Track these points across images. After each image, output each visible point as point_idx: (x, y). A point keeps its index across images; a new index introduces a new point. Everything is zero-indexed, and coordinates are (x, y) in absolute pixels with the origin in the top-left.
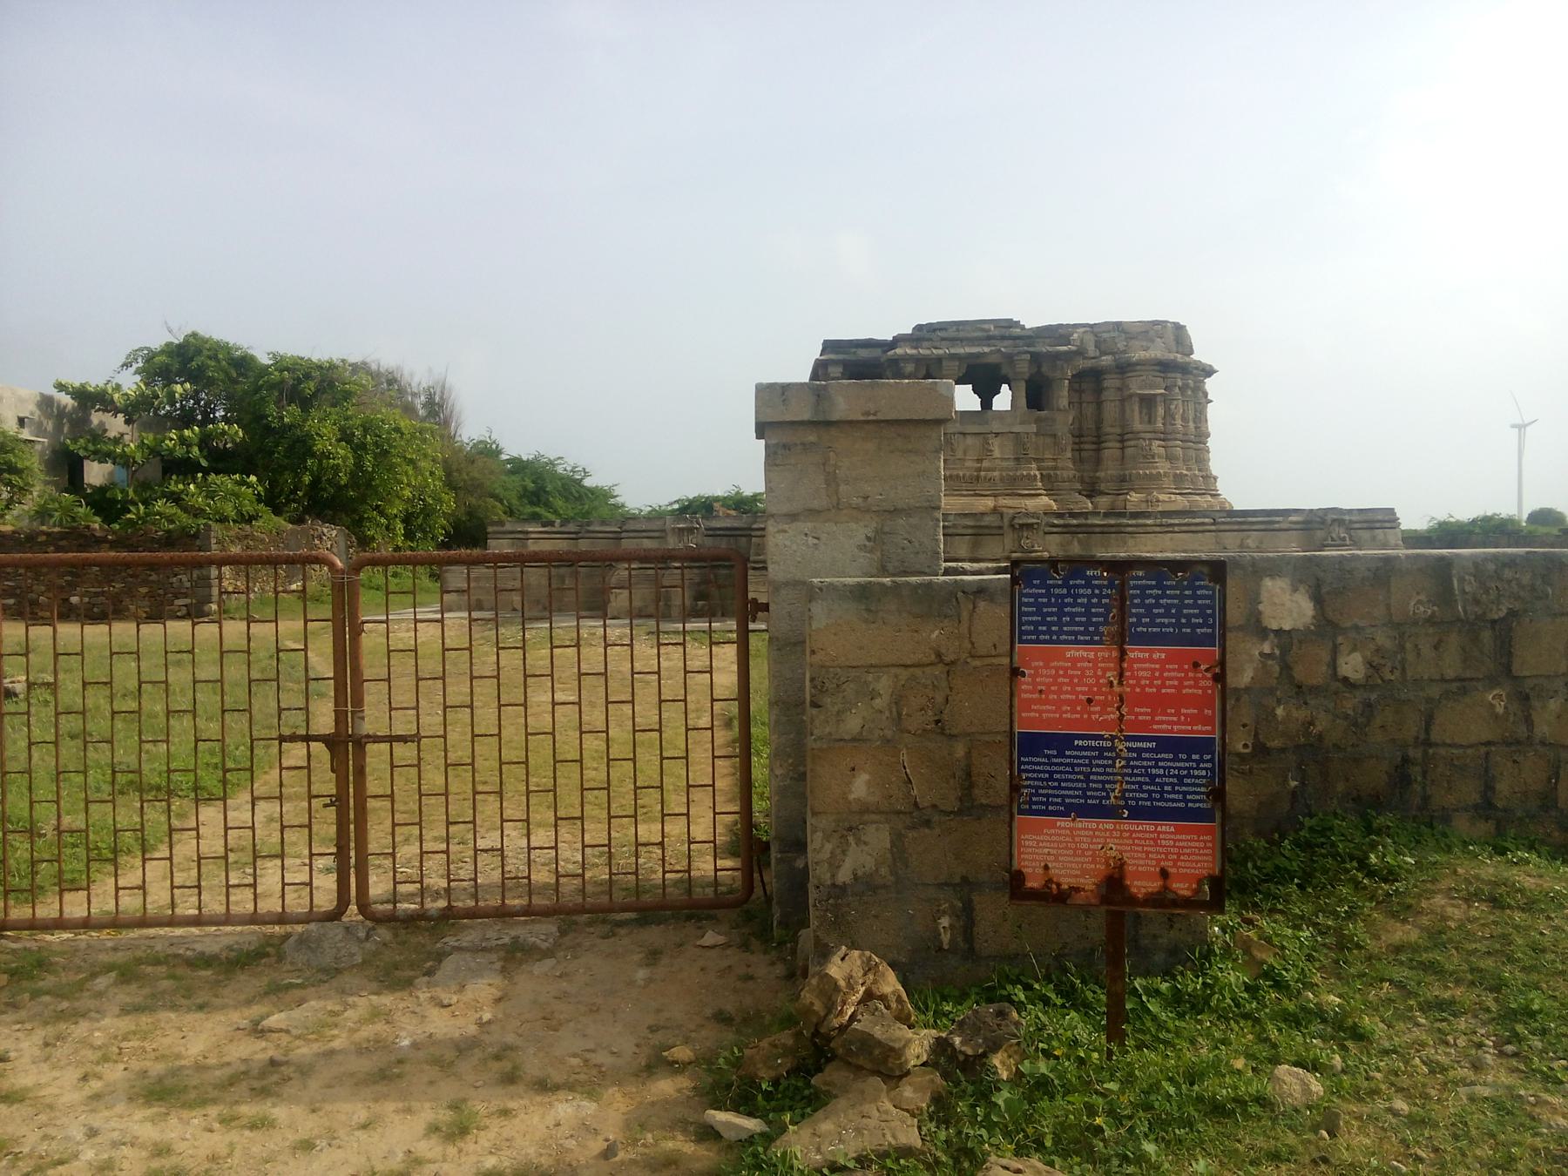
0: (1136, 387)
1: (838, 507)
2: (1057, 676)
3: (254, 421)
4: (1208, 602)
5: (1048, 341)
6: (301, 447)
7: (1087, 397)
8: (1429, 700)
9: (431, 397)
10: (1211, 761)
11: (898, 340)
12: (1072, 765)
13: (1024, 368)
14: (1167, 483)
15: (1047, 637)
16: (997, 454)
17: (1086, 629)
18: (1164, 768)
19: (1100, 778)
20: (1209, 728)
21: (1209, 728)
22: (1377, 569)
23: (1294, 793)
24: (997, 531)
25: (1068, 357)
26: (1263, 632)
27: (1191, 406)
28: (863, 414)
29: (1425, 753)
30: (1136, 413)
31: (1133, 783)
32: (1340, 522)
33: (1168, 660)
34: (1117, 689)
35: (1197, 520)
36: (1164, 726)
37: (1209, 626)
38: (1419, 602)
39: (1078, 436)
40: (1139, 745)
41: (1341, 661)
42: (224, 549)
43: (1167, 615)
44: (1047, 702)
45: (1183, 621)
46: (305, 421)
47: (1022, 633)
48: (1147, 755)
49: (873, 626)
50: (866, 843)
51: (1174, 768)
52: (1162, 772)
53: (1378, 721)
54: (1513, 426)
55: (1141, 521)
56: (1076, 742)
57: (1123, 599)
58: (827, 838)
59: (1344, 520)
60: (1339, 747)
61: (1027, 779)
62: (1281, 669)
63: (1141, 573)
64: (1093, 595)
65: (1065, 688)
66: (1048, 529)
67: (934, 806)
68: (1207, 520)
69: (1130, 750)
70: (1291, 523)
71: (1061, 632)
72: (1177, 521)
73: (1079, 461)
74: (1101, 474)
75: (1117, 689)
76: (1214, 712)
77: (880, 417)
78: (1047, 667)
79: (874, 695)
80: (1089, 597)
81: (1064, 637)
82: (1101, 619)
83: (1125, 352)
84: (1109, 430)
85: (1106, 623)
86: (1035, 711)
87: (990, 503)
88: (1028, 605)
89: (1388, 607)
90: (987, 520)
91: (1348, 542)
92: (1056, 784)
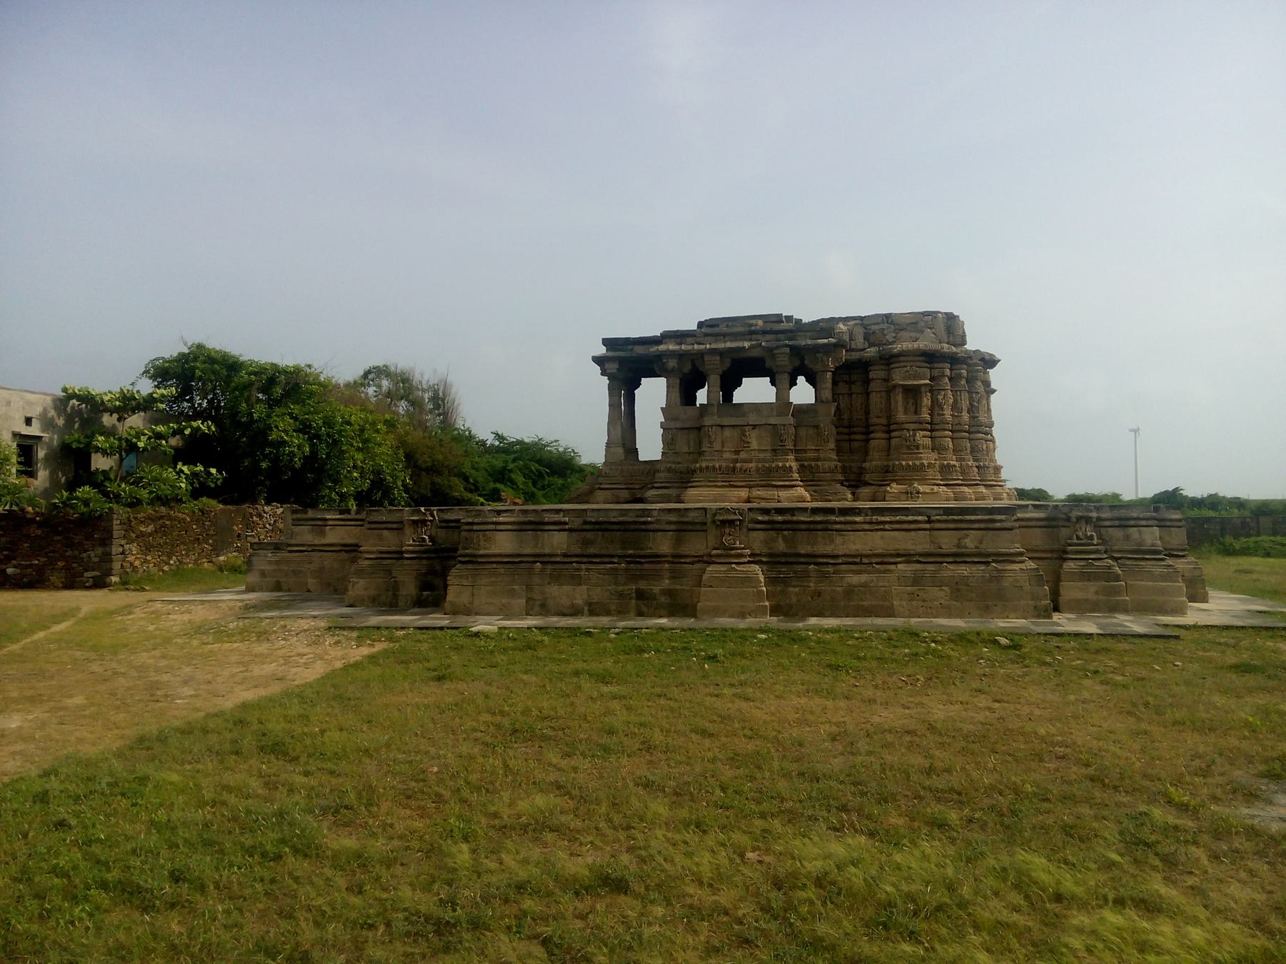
0: (899, 378)
5: (808, 334)
6: (259, 436)
9: (436, 392)
16: (754, 445)
25: (828, 349)
35: (910, 518)
46: (269, 416)
55: (849, 518)
66: (751, 526)
68: (920, 518)
72: (887, 519)
74: (867, 465)
84: (874, 420)
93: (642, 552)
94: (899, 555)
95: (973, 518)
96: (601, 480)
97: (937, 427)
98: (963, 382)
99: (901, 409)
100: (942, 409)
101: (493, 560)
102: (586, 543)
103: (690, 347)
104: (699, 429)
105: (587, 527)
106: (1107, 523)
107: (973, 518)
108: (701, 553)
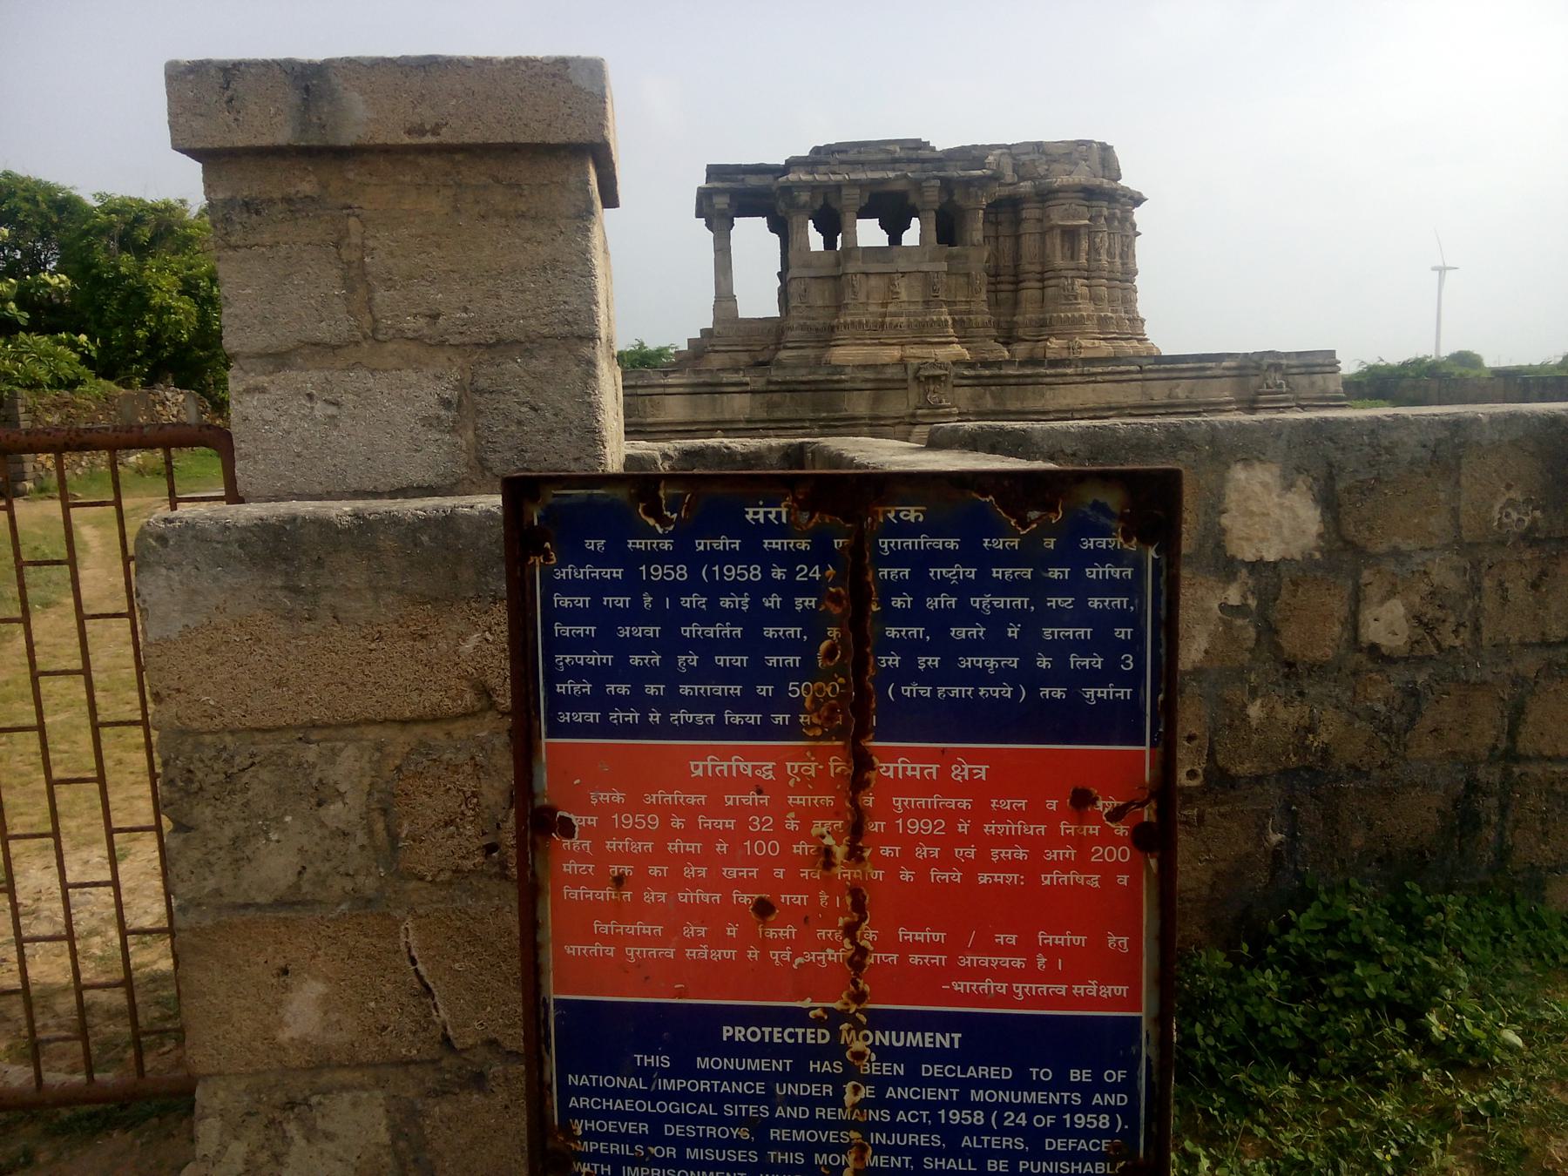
0: (1057, 218)
1: (374, 336)
2: (667, 833)
3: (78, 264)
4: (1119, 602)
6: (137, 300)
7: (1005, 229)
8: (1517, 680)
10: (1128, 1086)
11: (793, 164)
12: (718, 1099)
13: (933, 196)
14: (1091, 327)
15: (633, 716)
16: (904, 296)
17: (749, 691)
18: (986, 1107)
19: (801, 1136)
20: (1121, 990)
21: (1121, 990)
22: (1439, 442)
23: (1276, 854)
24: (900, 385)
25: (984, 182)
26: (1227, 567)
27: (1117, 239)
28: (409, 132)
29: (1507, 773)
30: (1058, 247)
31: (896, 1151)
32: (1277, 367)
33: (1000, 783)
34: (843, 872)
35: (1122, 368)
36: (987, 985)
37: (1122, 680)
38: (1511, 503)
39: (994, 275)
40: (914, 1039)
41: (1367, 615)
42: (36, 419)
43: (994, 644)
44: (639, 911)
45: (1043, 662)
46: (142, 270)
47: (558, 703)
48: (935, 1070)
49: (306, 628)
50: (329, 1136)
51: (1017, 1109)
52: (978, 1118)
53: (1424, 724)
54: (1434, 269)
55: (1060, 370)
56: (727, 1032)
57: (859, 596)
58: (235, 1129)
59: (1281, 365)
60: (1358, 770)
61: (589, 1135)
62: (1259, 634)
63: (912, 514)
64: (768, 586)
65: (690, 872)
66: (957, 382)
67: (492, 1043)
68: (1132, 368)
69: (884, 1053)
70: (1224, 368)
71: (672, 701)
73: (994, 303)
74: (1018, 318)
75: (843, 872)
76: (1135, 945)
77: (446, 137)
78: (635, 805)
79: (322, 795)
80: (758, 590)
81: (680, 716)
82: (793, 660)
83: (1045, 177)
84: (1028, 267)
85: (808, 671)
86: (606, 940)
87: (896, 353)
88: (572, 616)
89: (1455, 512)
90: (890, 373)
91: (1285, 389)
92: (670, 1152)
93: (837, 415)
94: (1110, 409)
95: (1184, 366)
96: (714, 341)
97: (1093, 274)
98: (1103, 221)
99: (1058, 253)
100: (1099, 254)
101: (664, 428)
102: (771, 406)
103: (824, 178)
104: (837, 278)
105: (772, 387)
106: (1294, 371)
107: (1184, 366)
108: (902, 414)
